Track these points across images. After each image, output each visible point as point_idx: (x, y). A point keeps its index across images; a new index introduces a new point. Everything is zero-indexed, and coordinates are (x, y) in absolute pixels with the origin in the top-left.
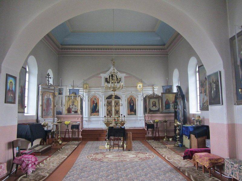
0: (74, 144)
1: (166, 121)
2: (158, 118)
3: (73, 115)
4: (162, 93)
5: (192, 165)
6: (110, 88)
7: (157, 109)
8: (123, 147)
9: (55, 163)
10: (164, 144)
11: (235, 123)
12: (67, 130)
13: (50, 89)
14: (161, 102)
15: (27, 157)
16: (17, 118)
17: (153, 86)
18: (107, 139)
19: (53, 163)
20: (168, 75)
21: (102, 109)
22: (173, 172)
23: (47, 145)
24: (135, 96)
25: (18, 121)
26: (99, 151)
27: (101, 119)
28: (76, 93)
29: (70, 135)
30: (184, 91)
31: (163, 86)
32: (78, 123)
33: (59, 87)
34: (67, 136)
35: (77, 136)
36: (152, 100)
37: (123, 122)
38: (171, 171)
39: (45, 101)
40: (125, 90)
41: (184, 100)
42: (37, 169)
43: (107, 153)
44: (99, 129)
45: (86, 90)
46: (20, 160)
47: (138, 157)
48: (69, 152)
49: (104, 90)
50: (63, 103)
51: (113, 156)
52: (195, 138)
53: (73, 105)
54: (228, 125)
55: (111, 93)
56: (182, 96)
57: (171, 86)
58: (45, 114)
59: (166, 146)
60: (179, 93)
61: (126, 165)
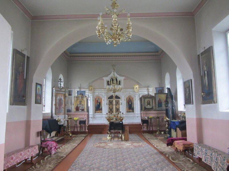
0: (82, 136)
1: (158, 118)
2: (152, 115)
3: (80, 112)
4: (155, 94)
5: (174, 150)
6: (111, 90)
7: (151, 107)
8: (121, 138)
9: (52, 164)
10: (156, 136)
11: (202, 117)
12: (76, 125)
13: (61, 91)
14: (155, 101)
15: (50, 143)
16: (42, 115)
17: (148, 87)
18: (109, 132)
19: (67, 149)
20: (161, 79)
21: (105, 108)
22: (158, 155)
23: (60, 137)
24: (133, 96)
25: (43, 117)
26: (103, 141)
27: (104, 116)
28: (82, 94)
29: (79, 129)
30: (173, 93)
31: (156, 88)
32: (85, 119)
33: (69, 90)
34: (76, 130)
35: (84, 130)
36: (147, 100)
37: (122, 118)
38: (156, 154)
39: (58, 101)
40: (124, 91)
41: (173, 99)
42: (57, 152)
43: (108, 143)
44: (102, 124)
45: (91, 91)
46: (46, 144)
47: (133, 145)
48: (78, 141)
49: (106, 91)
50: (72, 102)
51: (113, 145)
52: (180, 131)
53: (80, 104)
54: (197, 119)
55: (111, 93)
56: (171, 96)
57: (163, 87)
58: (58, 112)
59: (158, 137)
60: (169, 94)
61: (125, 156)
